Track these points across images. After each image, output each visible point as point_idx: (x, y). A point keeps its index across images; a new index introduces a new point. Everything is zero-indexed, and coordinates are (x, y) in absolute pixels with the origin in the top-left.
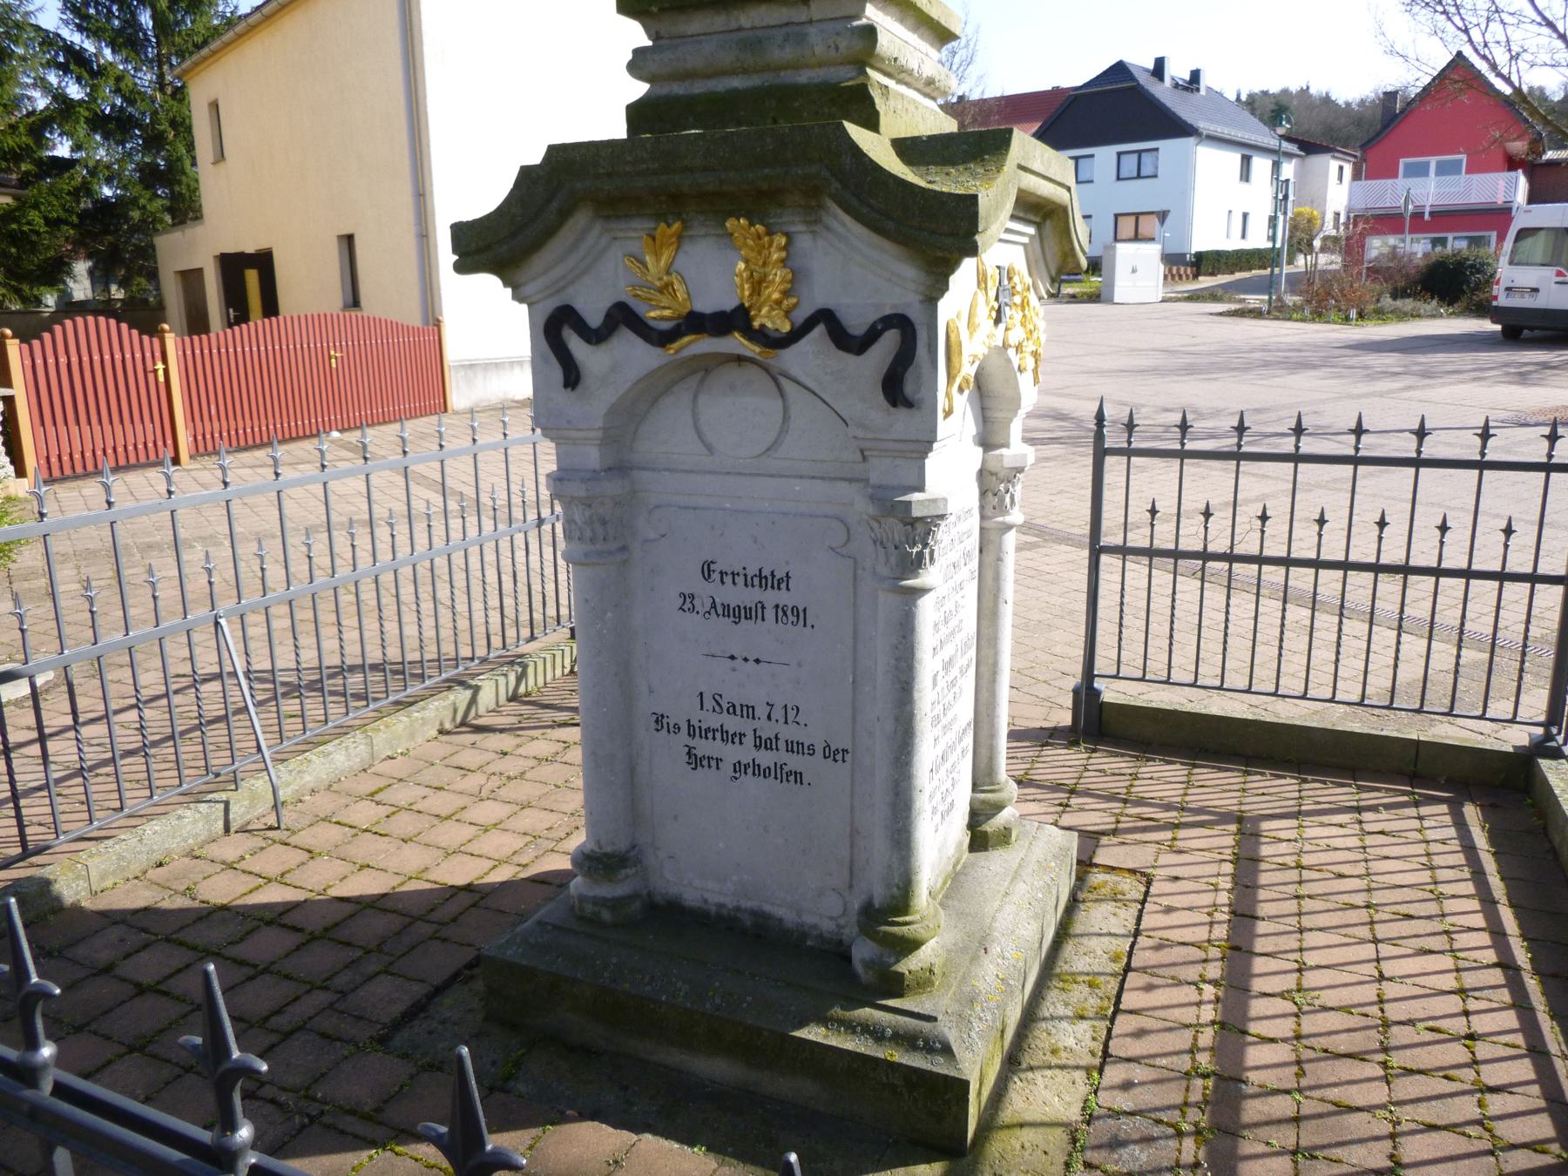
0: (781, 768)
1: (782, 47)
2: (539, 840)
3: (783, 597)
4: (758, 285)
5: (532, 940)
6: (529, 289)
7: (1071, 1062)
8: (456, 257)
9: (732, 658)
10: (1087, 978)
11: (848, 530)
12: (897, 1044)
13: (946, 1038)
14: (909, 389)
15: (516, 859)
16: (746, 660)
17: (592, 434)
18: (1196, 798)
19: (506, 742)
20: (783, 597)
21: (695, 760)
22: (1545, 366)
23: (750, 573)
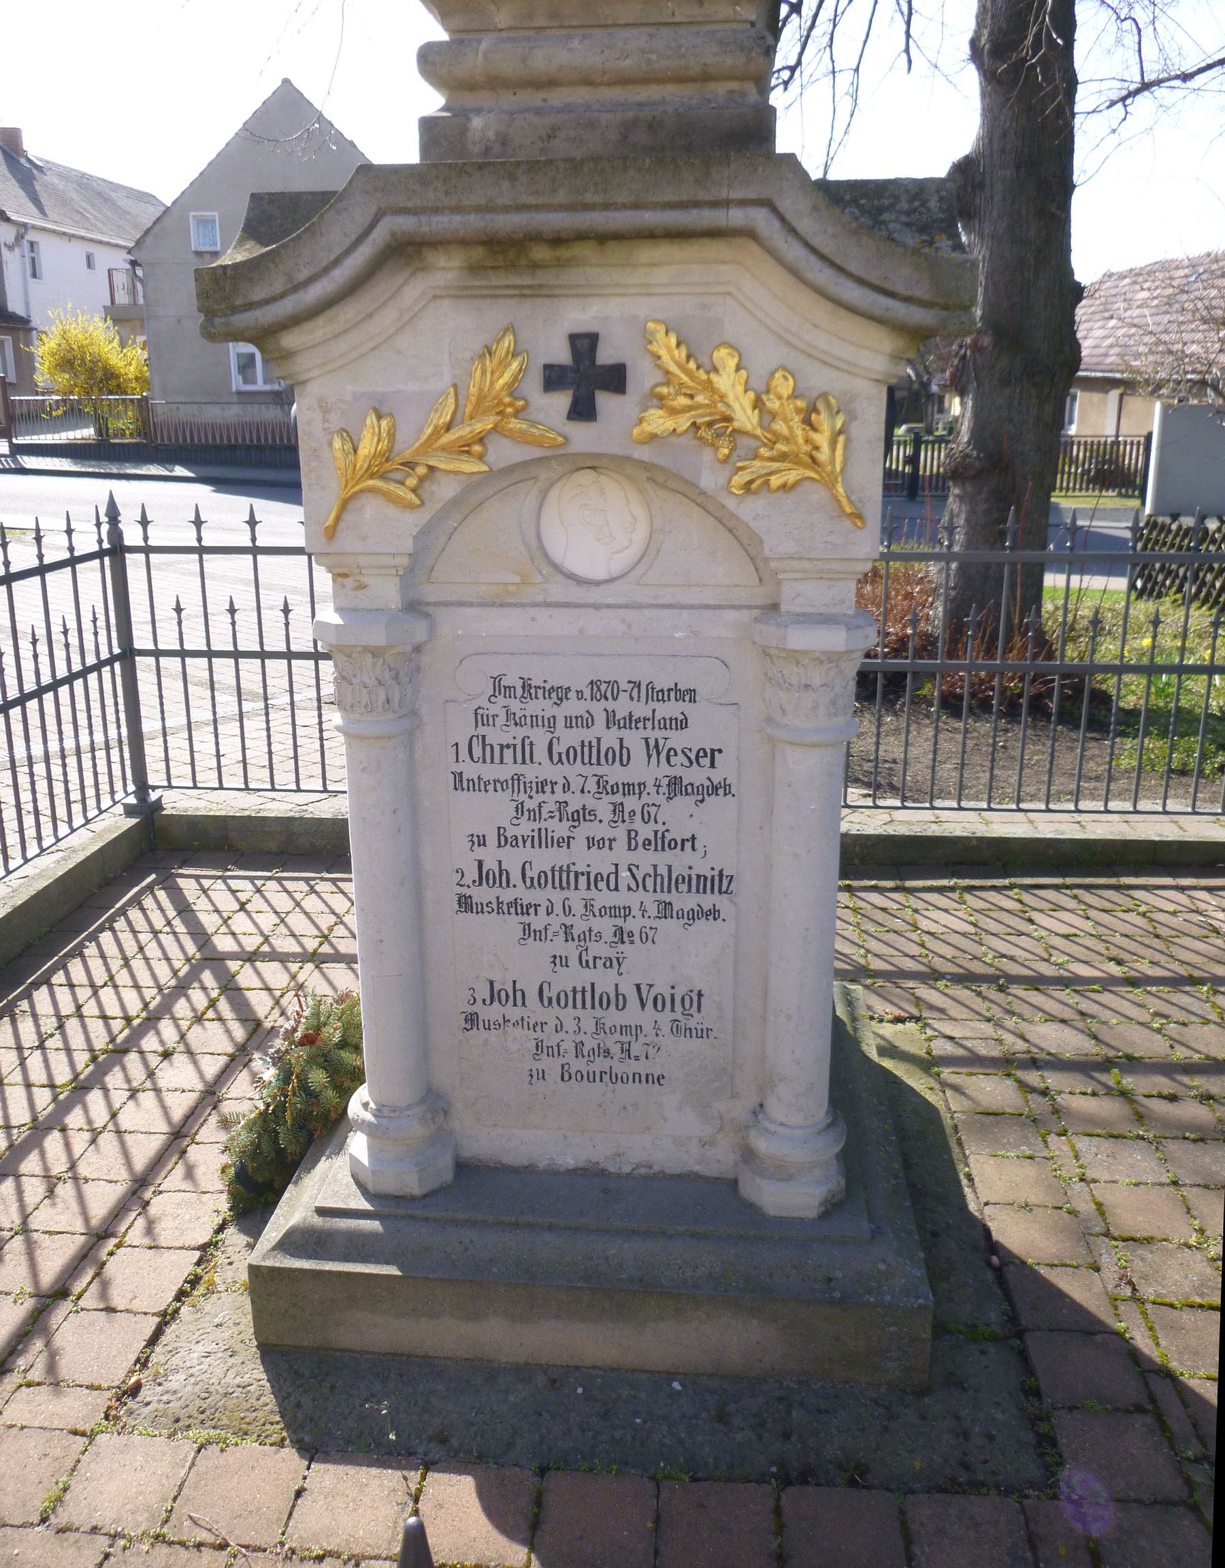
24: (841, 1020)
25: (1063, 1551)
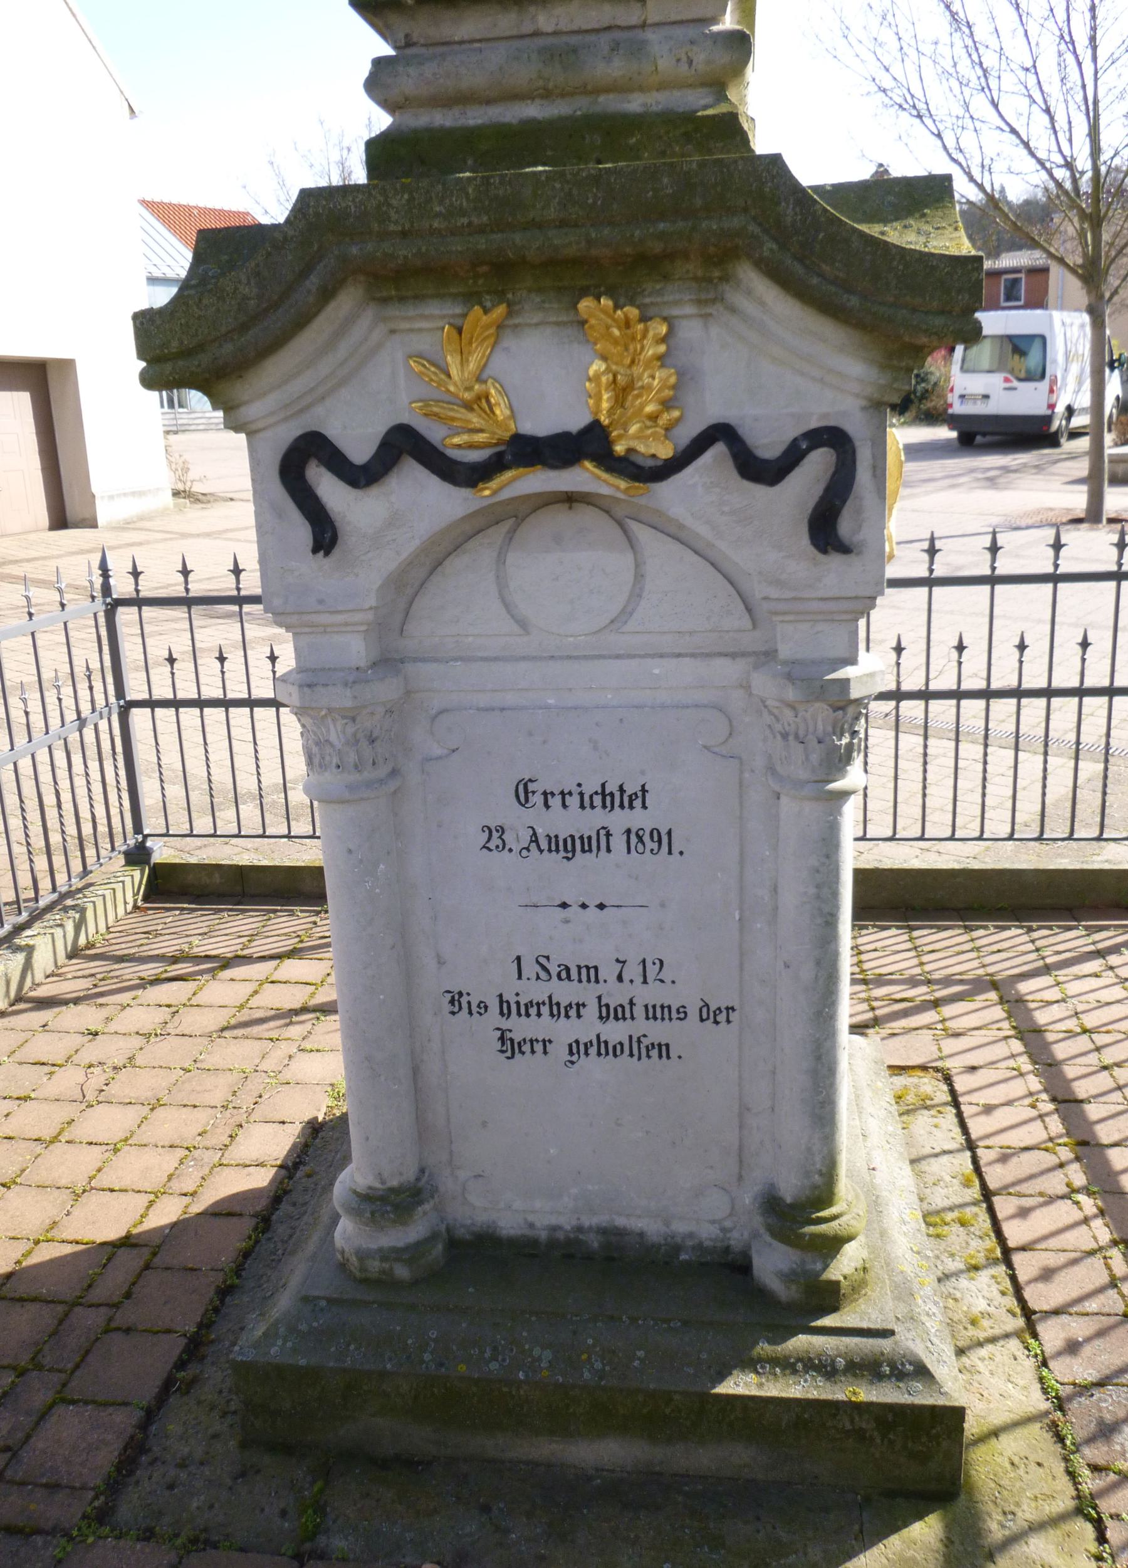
0: (639, 1041)
1: (608, 60)
2: (196, 1153)
3: (637, 819)
4: (623, 392)
5: (303, 1327)
6: (253, 411)
7: (997, 1331)
8: (143, 364)
9: (564, 905)
10: (955, 1214)
11: (730, 721)
12: (855, 1375)
13: (916, 1355)
14: (845, 527)
15: (176, 1186)
16: (584, 906)
17: (358, 617)
18: (938, 967)
19: (87, 1016)
20: (637, 819)
21: (510, 1046)
22: (1006, 470)
23: (588, 790)
24: (785, 1339)
25: (33, 1507)
